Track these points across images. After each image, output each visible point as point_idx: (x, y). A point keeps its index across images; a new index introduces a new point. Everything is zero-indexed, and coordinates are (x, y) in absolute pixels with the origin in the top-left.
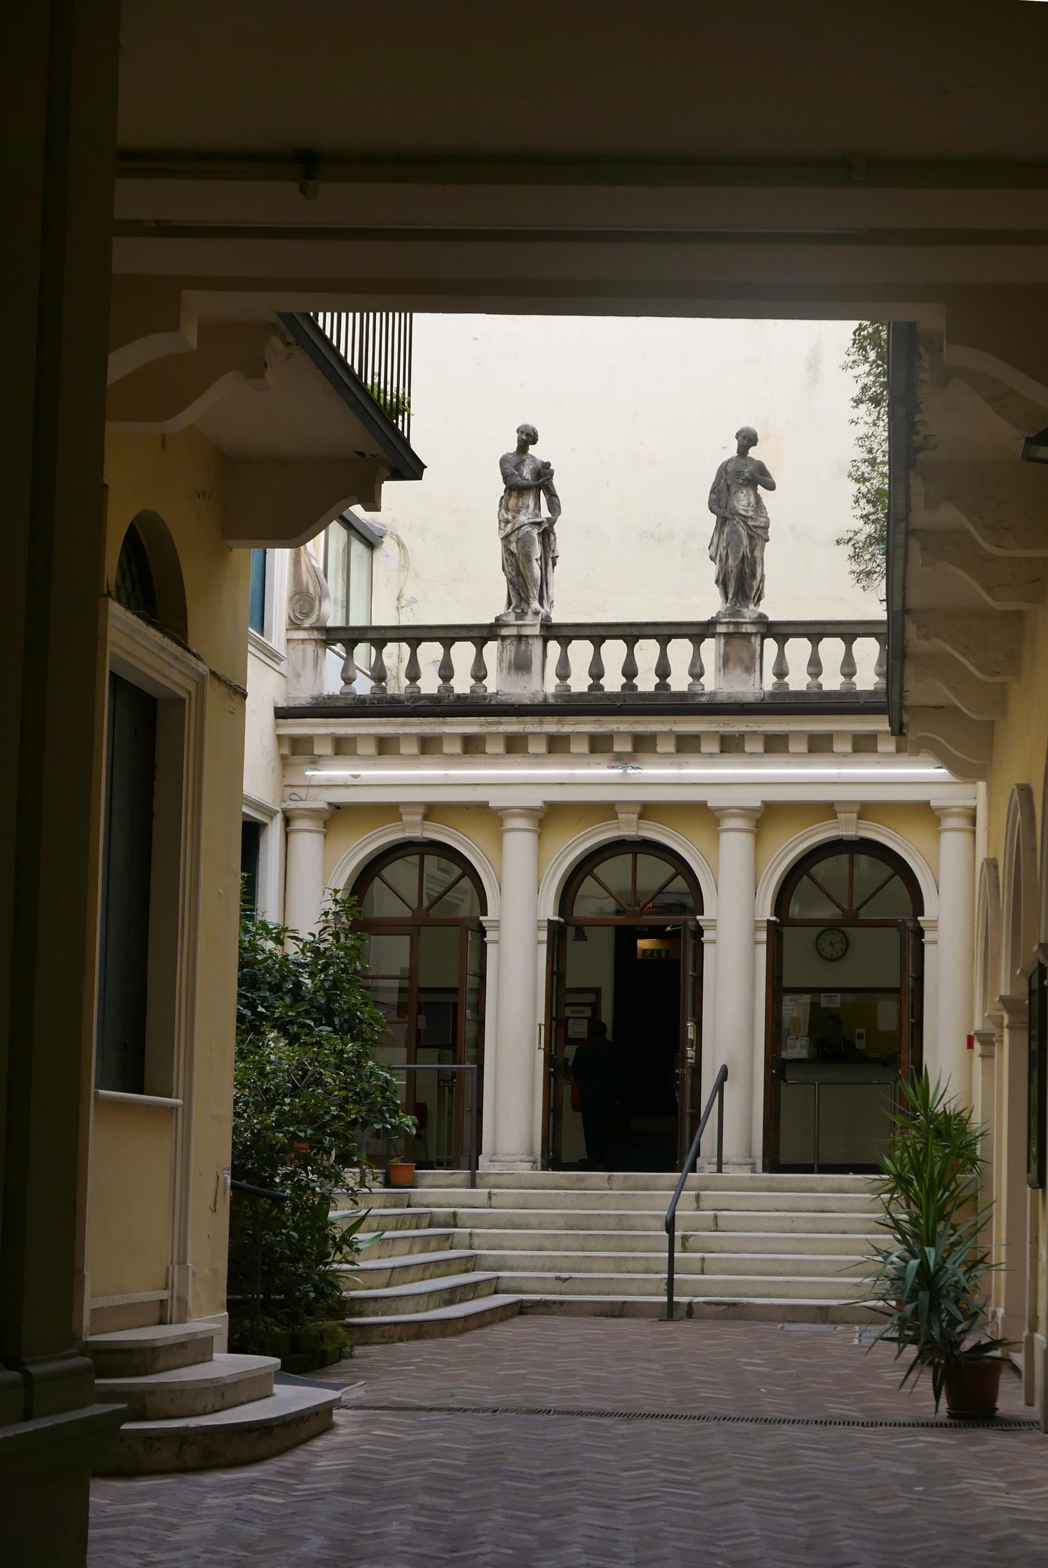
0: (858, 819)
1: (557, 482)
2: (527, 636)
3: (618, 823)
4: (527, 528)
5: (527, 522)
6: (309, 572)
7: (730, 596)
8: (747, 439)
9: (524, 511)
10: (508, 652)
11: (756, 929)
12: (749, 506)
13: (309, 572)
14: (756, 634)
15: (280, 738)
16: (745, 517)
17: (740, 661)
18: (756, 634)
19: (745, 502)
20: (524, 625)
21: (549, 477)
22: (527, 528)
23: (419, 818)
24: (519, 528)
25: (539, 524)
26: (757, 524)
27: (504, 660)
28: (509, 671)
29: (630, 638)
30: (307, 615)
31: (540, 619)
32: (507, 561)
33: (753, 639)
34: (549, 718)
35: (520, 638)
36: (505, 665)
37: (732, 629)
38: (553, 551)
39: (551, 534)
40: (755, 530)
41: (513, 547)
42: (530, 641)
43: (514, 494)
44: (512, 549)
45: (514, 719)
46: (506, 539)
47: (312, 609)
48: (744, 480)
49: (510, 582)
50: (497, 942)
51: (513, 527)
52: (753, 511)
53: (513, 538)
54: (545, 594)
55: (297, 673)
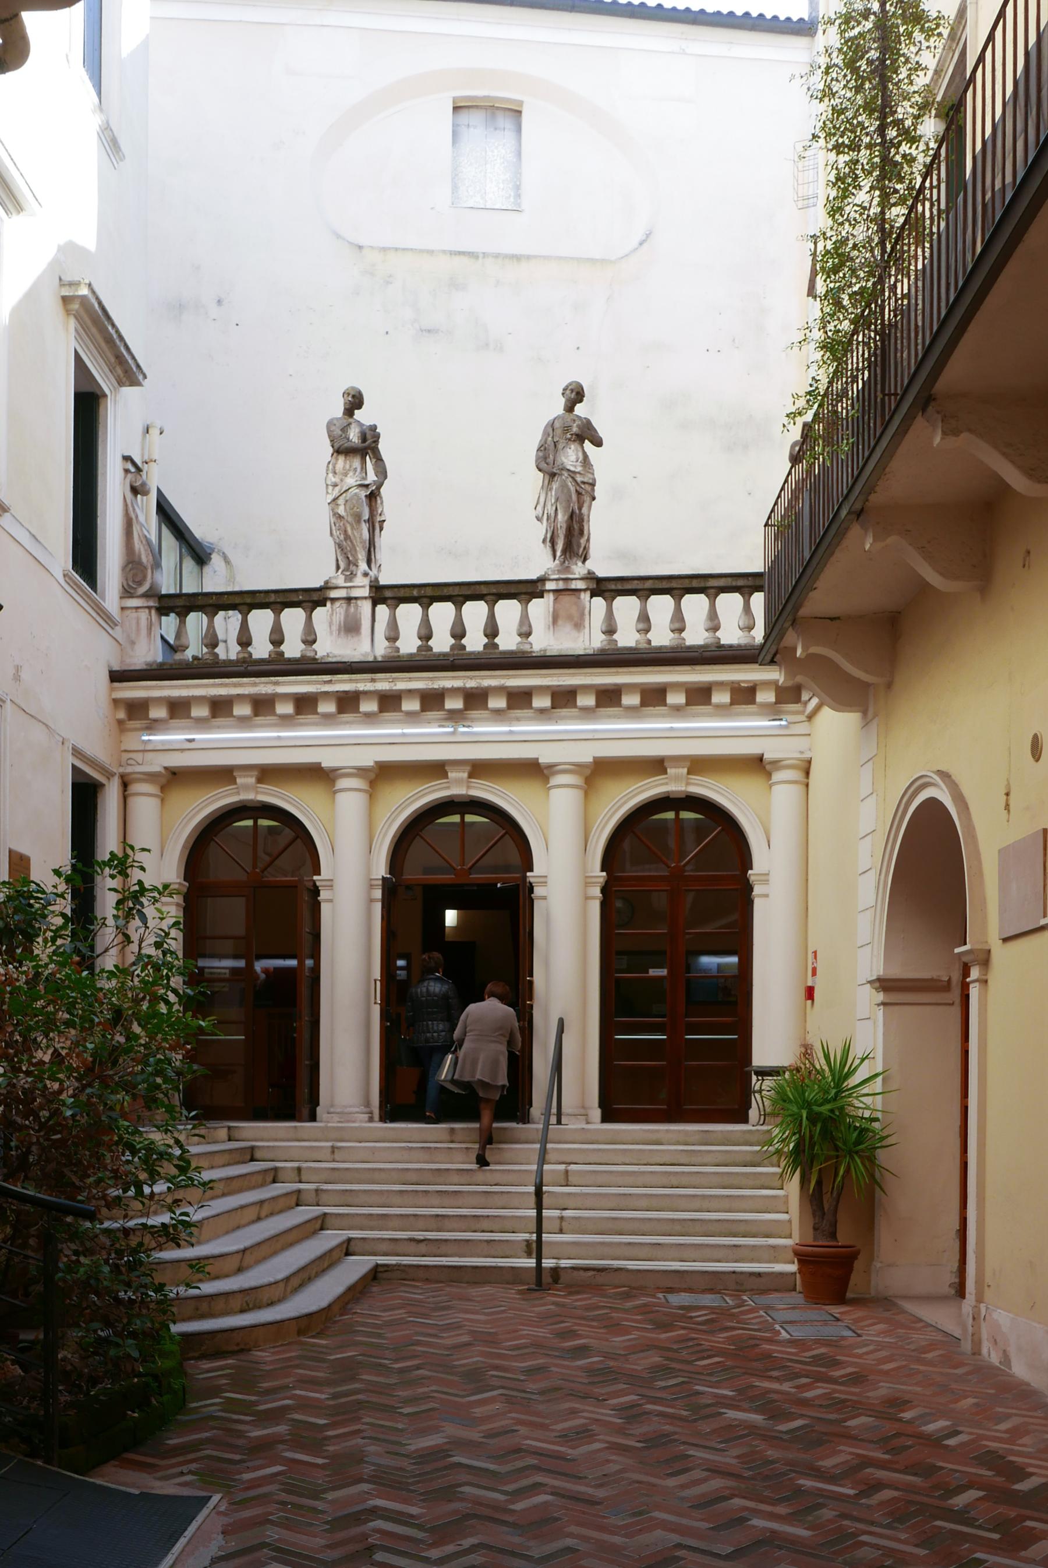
2: (356, 598)
12: (577, 461)
14: (585, 590)
16: (574, 472)
17: (570, 618)
18: (585, 590)
25: (367, 486)
26: (586, 480)
27: (334, 622)
30: (140, 583)
36: (335, 628)
37: (561, 585)
41: (341, 510)
42: (359, 602)
44: (339, 512)
47: (145, 577)
49: (339, 546)
53: (341, 501)
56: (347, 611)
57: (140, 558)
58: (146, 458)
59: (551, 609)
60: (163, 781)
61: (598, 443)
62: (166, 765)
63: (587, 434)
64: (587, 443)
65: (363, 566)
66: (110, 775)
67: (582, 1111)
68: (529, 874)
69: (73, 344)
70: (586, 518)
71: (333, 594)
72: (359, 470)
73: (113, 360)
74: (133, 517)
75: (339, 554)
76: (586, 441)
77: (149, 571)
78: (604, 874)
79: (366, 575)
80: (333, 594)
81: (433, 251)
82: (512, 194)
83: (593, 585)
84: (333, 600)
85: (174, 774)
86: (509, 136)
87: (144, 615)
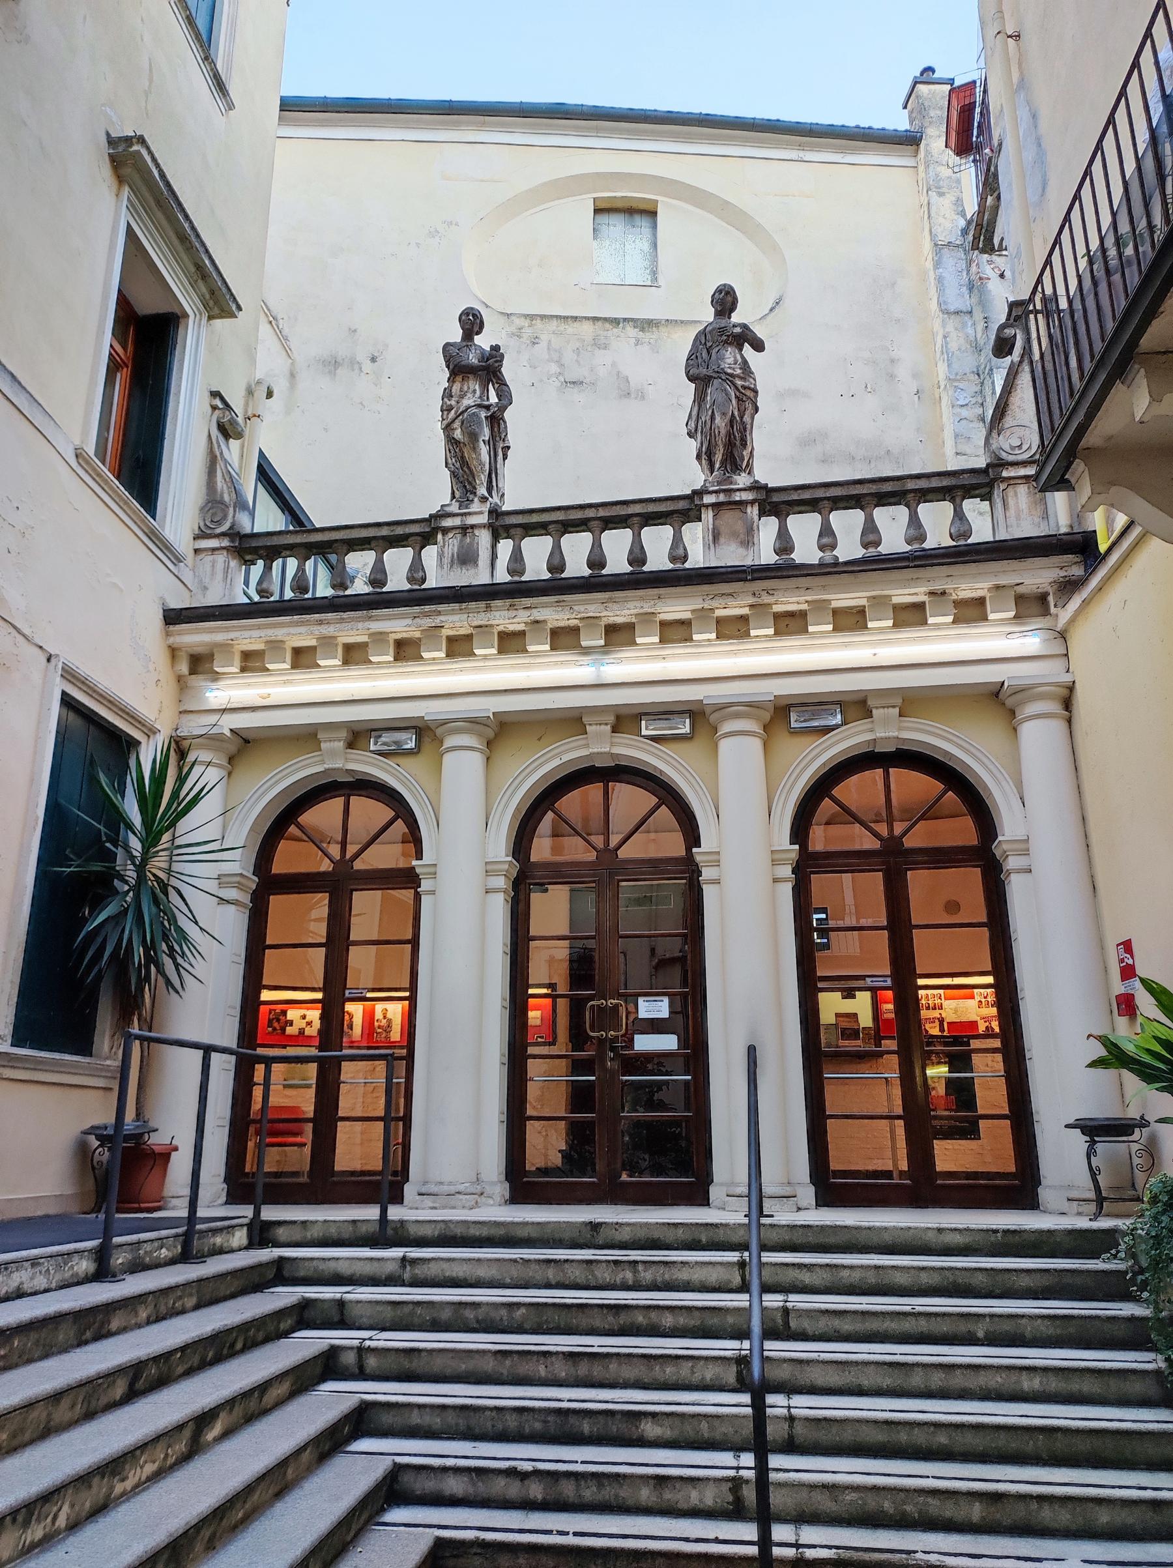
0: (900, 716)
1: (507, 371)
2: (473, 527)
3: (587, 738)
4: (474, 410)
5: (473, 404)
6: (225, 480)
7: (717, 465)
8: (725, 301)
9: (469, 395)
10: (450, 547)
11: (774, 863)
12: (735, 364)
13: (225, 480)
14: (752, 502)
15: (173, 651)
16: (731, 375)
17: (734, 535)
18: (752, 502)
19: (731, 360)
20: (470, 514)
21: (499, 359)
22: (474, 410)
23: (341, 745)
24: (463, 412)
25: (488, 408)
26: (747, 384)
27: (446, 554)
28: (451, 566)
29: (596, 522)
30: (219, 523)
31: (488, 507)
32: (450, 452)
33: (749, 509)
34: (498, 603)
35: (465, 530)
36: (446, 561)
37: (722, 498)
38: (504, 440)
39: (501, 421)
40: (743, 391)
41: (458, 434)
42: (477, 532)
43: (459, 378)
44: (455, 436)
45: (456, 606)
46: (448, 428)
47: (225, 517)
48: (728, 336)
49: (454, 475)
50: (433, 892)
51: (456, 413)
52: (740, 368)
53: (457, 424)
54: (494, 484)
55: (205, 587)
56: (461, 541)
57: (222, 496)
58: (250, 414)
59: (711, 527)
60: (233, 748)
61: (758, 346)
62: (232, 727)
63: (745, 338)
64: (747, 347)
65: (482, 491)
66: (151, 732)
67: (787, 1191)
68: (695, 850)
69: (124, 217)
70: (748, 426)
71: (448, 523)
72: (478, 393)
73: (193, 269)
74: (218, 454)
75: (454, 484)
76: (746, 344)
77: (231, 510)
78: (797, 847)
79: (484, 499)
80: (448, 523)
81: (576, 317)
82: (650, 279)
83: (762, 495)
84: (445, 531)
85: (247, 741)
86: (646, 231)
87: (221, 558)
